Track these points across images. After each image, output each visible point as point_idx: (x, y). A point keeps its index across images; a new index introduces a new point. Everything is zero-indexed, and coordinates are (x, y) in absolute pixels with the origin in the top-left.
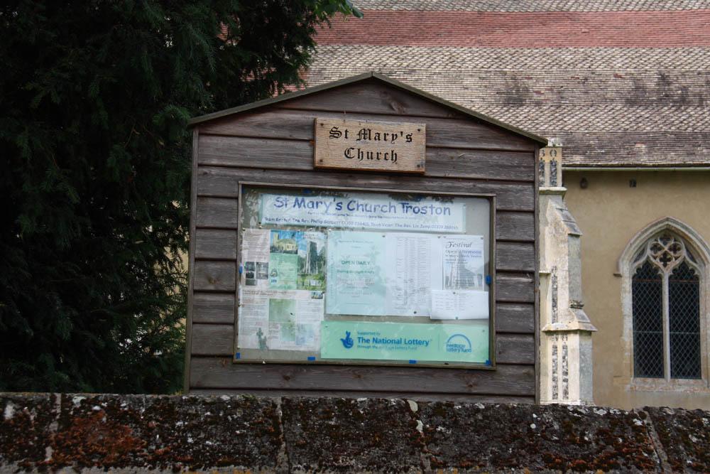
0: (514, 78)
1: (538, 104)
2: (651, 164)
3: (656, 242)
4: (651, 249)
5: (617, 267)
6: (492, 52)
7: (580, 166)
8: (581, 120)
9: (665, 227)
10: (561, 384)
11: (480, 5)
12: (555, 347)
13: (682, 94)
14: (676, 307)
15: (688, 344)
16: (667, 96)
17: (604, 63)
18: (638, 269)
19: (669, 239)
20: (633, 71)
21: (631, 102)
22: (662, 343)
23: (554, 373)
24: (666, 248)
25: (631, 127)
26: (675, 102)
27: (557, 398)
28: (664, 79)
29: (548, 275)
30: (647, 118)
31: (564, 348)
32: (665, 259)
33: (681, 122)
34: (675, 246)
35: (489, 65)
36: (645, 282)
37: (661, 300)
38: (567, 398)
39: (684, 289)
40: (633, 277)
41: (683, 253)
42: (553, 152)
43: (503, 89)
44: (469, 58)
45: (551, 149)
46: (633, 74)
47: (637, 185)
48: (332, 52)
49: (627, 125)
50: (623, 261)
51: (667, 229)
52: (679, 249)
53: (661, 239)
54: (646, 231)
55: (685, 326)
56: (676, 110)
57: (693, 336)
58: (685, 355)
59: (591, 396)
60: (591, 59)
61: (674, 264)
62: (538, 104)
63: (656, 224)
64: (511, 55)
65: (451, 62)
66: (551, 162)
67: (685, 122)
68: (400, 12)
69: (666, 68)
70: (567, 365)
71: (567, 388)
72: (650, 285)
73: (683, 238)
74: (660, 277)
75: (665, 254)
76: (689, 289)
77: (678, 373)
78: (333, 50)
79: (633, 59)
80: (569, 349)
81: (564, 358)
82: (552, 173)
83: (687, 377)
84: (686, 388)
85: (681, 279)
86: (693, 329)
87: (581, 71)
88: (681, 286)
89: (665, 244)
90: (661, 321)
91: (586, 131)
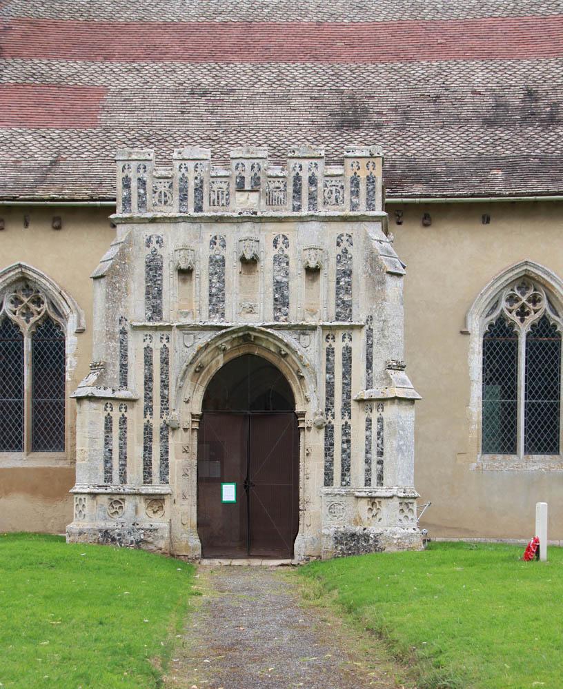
0: (352, 98)
1: (378, 126)
2: (507, 193)
3: (511, 292)
4: (507, 300)
6: (329, 68)
7: (421, 196)
8: (428, 144)
9: (523, 273)
10: (374, 466)
11: (320, 15)
12: (369, 421)
13: (551, 113)
14: (534, 370)
15: (546, 414)
16: (533, 114)
17: (460, 78)
18: (491, 326)
19: (528, 288)
20: (494, 86)
21: (489, 122)
22: (516, 414)
23: (367, 453)
24: (524, 300)
25: (487, 151)
26: (542, 121)
27: (370, 485)
28: (531, 95)
29: (361, 327)
30: (507, 140)
31: (379, 422)
32: (523, 313)
33: (548, 144)
34: (535, 296)
35: (323, 83)
36: (498, 343)
37: (516, 362)
38: (382, 485)
39: (544, 349)
40: (484, 336)
41: (544, 304)
42: (371, 164)
43: (337, 109)
44: (301, 76)
45: (367, 160)
46: (494, 90)
47: (491, 222)
48: (137, 70)
49: (483, 148)
50: (472, 314)
51: (525, 275)
52: (539, 300)
53: (519, 288)
54: (501, 277)
55: (543, 392)
56: (542, 131)
57: (552, 405)
58: (542, 427)
59: (412, 481)
60: (445, 74)
61: (532, 318)
62: (378, 126)
63: (512, 270)
64: (351, 71)
65: (279, 80)
66: (368, 178)
67: (553, 144)
68: (224, 24)
69: (535, 82)
70: (382, 443)
71: (382, 471)
72: (504, 345)
73: (544, 286)
74: (517, 336)
75: (523, 307)
76: (550, 349)
77: (533, 449)
78: (138, 67)
79: (495, 72)
80: (385, 423)
81: (379, 434)
82: (368, 192)
83: (542, 453)
84: (541, 465)
85: (541, 336)
86: (552, 396)
87: (432, 89)
88: (541, 344)
89: (523, 294)
90: (516, 388)
91: (433, 157)
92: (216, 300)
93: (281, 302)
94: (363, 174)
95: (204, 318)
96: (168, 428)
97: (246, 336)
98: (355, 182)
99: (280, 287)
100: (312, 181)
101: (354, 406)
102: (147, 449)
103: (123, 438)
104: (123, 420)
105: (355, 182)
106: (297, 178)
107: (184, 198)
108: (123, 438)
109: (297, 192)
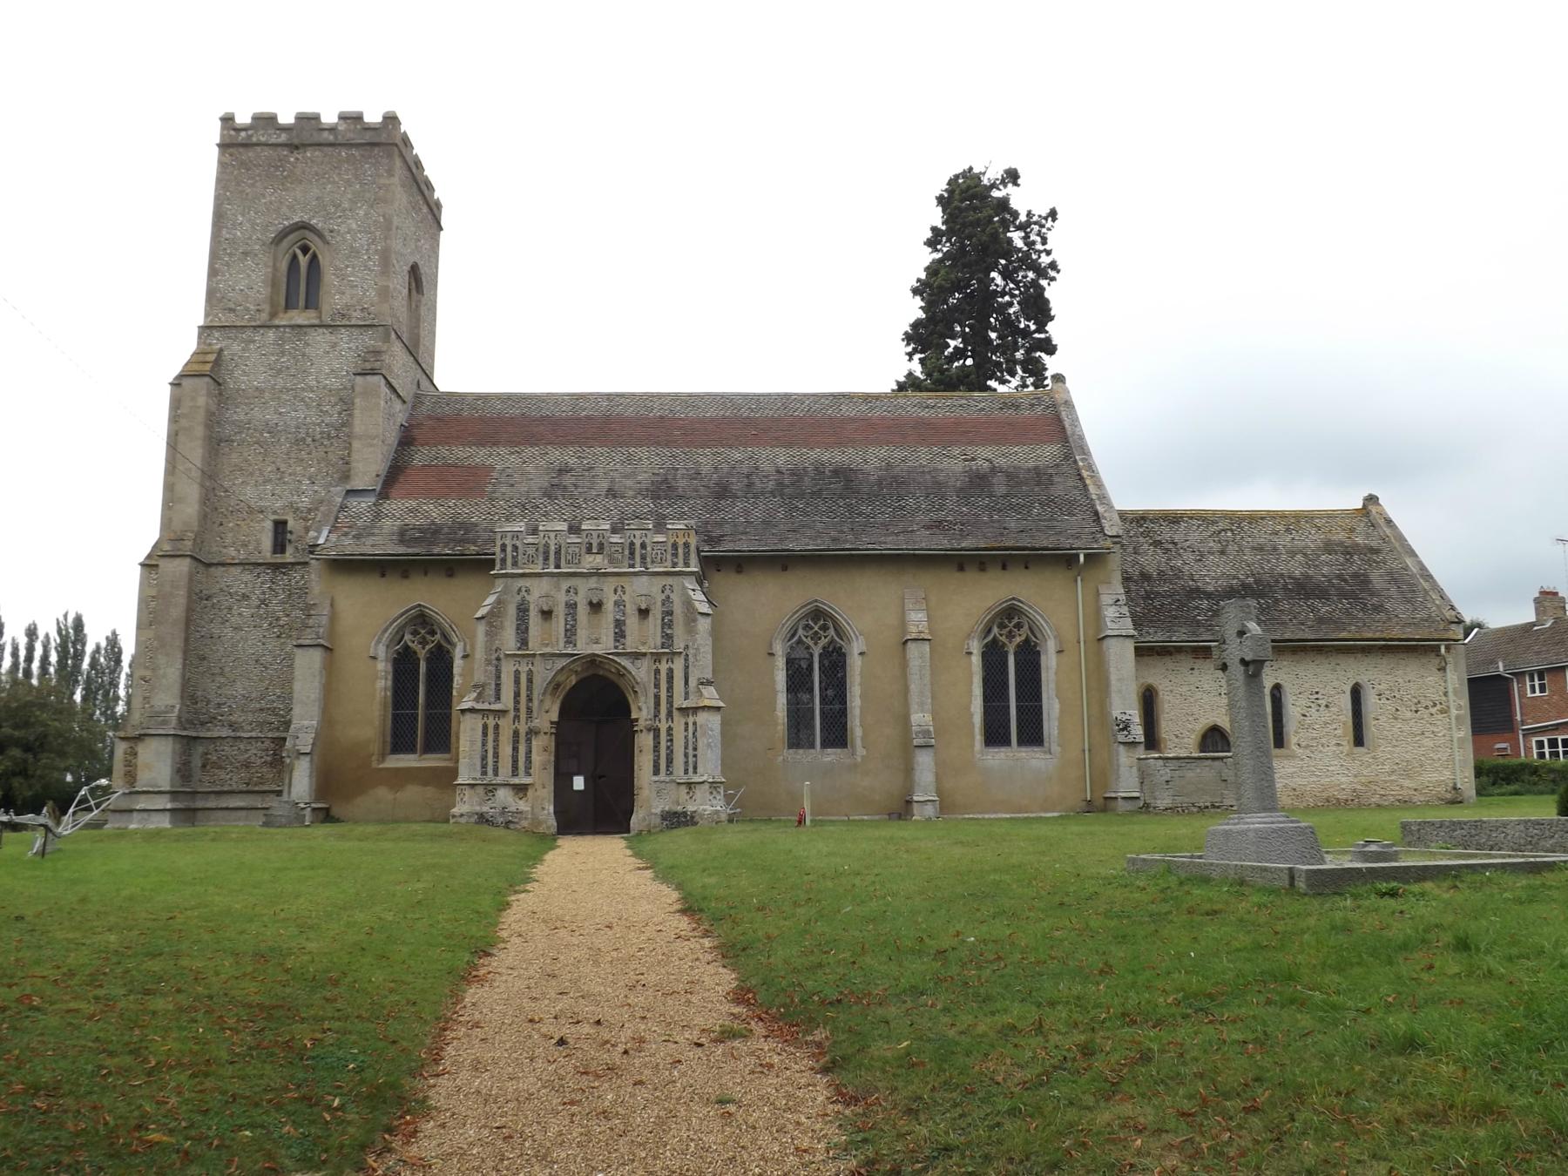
5: (771, 645)
10: (691, 759)
36: (403, 664)
41: (832, 632)
61: (823, 642)
92: (570, 634)
93: (620, 635)
94: (681, 541)
95: (560, 648)
96: (532, 733)
97: (593, 661)
98: (675, 546)
99: (619, 624)
100: (643, 546)
101: (675, 713)
102: (515, 749)
103: (496, 740)
104: (497, 727)
105: (675, 546)
106: (632, 544)
107: (546, 559)
108: (496, 740)
109: (632, 553)
